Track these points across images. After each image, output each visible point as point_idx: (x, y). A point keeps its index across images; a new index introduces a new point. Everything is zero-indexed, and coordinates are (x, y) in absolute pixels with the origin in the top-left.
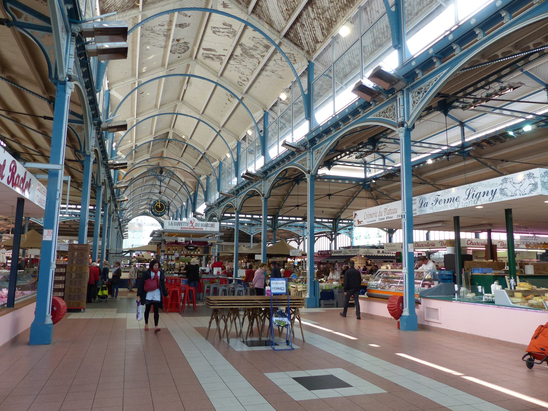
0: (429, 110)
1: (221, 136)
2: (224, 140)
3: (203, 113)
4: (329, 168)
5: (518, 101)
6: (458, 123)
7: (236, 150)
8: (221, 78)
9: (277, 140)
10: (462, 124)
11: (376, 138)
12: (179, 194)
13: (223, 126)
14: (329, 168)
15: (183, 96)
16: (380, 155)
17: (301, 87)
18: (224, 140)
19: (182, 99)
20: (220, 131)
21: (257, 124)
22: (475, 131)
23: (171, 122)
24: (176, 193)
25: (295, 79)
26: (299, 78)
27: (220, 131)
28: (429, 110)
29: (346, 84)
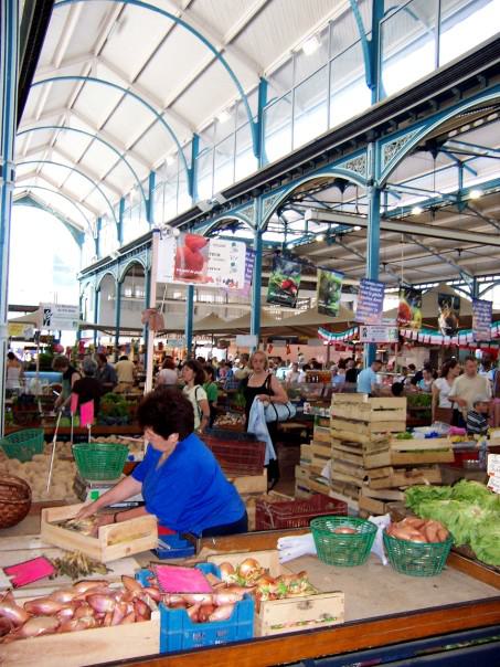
0: (418, 149)
1: (163, 121)
2: (168, 127)
3: (135, 80)
4: (234, 232)
5: (348, 203)
6: (455, 162)
7: (119, 206)
8: (188, 11)
9: (326, 97)
10: (460, 164)
11: (440, 139)
12: (128, 158)
13: (232, 42)
14: (234, 232)
15: (102, 48)
16: (455, 159)
17: (359, 20)
18: (168, 127)
19: (99, 54)
20: (223, 51)
21: (181, 149)
22: (476, 174)
23: (69, 100)
24: (96, 182)
25: (240, 97)
26: (245, 98)
27: (223, 51)
28: (418, 149)
29: (309, 111)
